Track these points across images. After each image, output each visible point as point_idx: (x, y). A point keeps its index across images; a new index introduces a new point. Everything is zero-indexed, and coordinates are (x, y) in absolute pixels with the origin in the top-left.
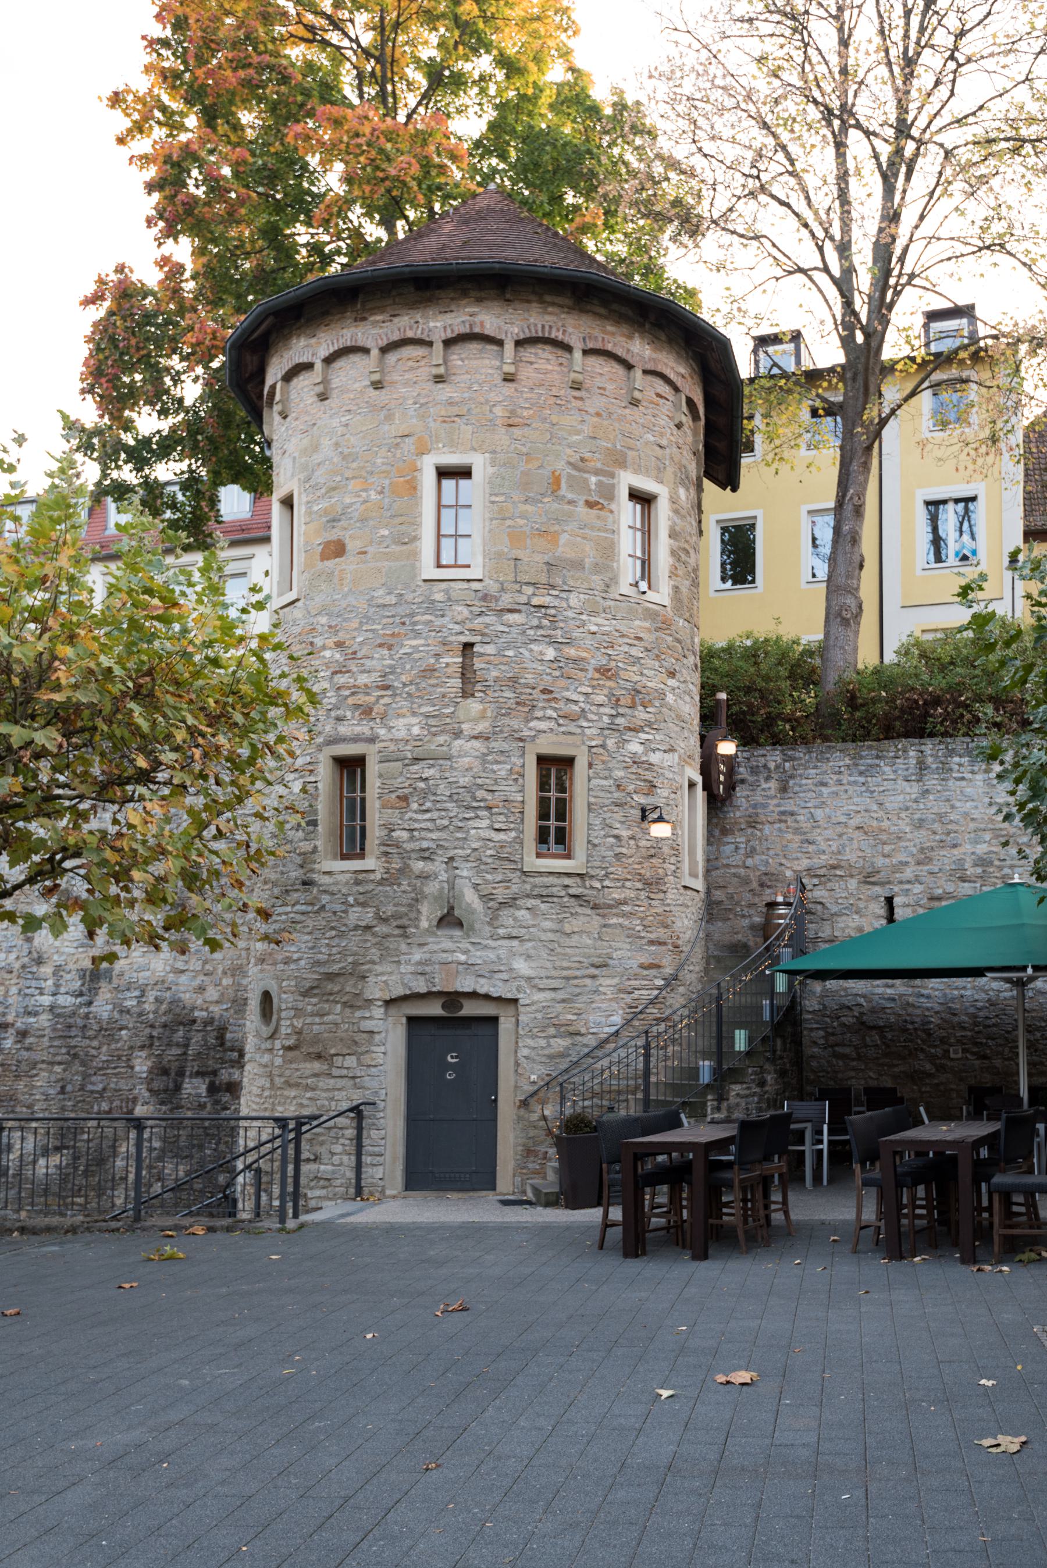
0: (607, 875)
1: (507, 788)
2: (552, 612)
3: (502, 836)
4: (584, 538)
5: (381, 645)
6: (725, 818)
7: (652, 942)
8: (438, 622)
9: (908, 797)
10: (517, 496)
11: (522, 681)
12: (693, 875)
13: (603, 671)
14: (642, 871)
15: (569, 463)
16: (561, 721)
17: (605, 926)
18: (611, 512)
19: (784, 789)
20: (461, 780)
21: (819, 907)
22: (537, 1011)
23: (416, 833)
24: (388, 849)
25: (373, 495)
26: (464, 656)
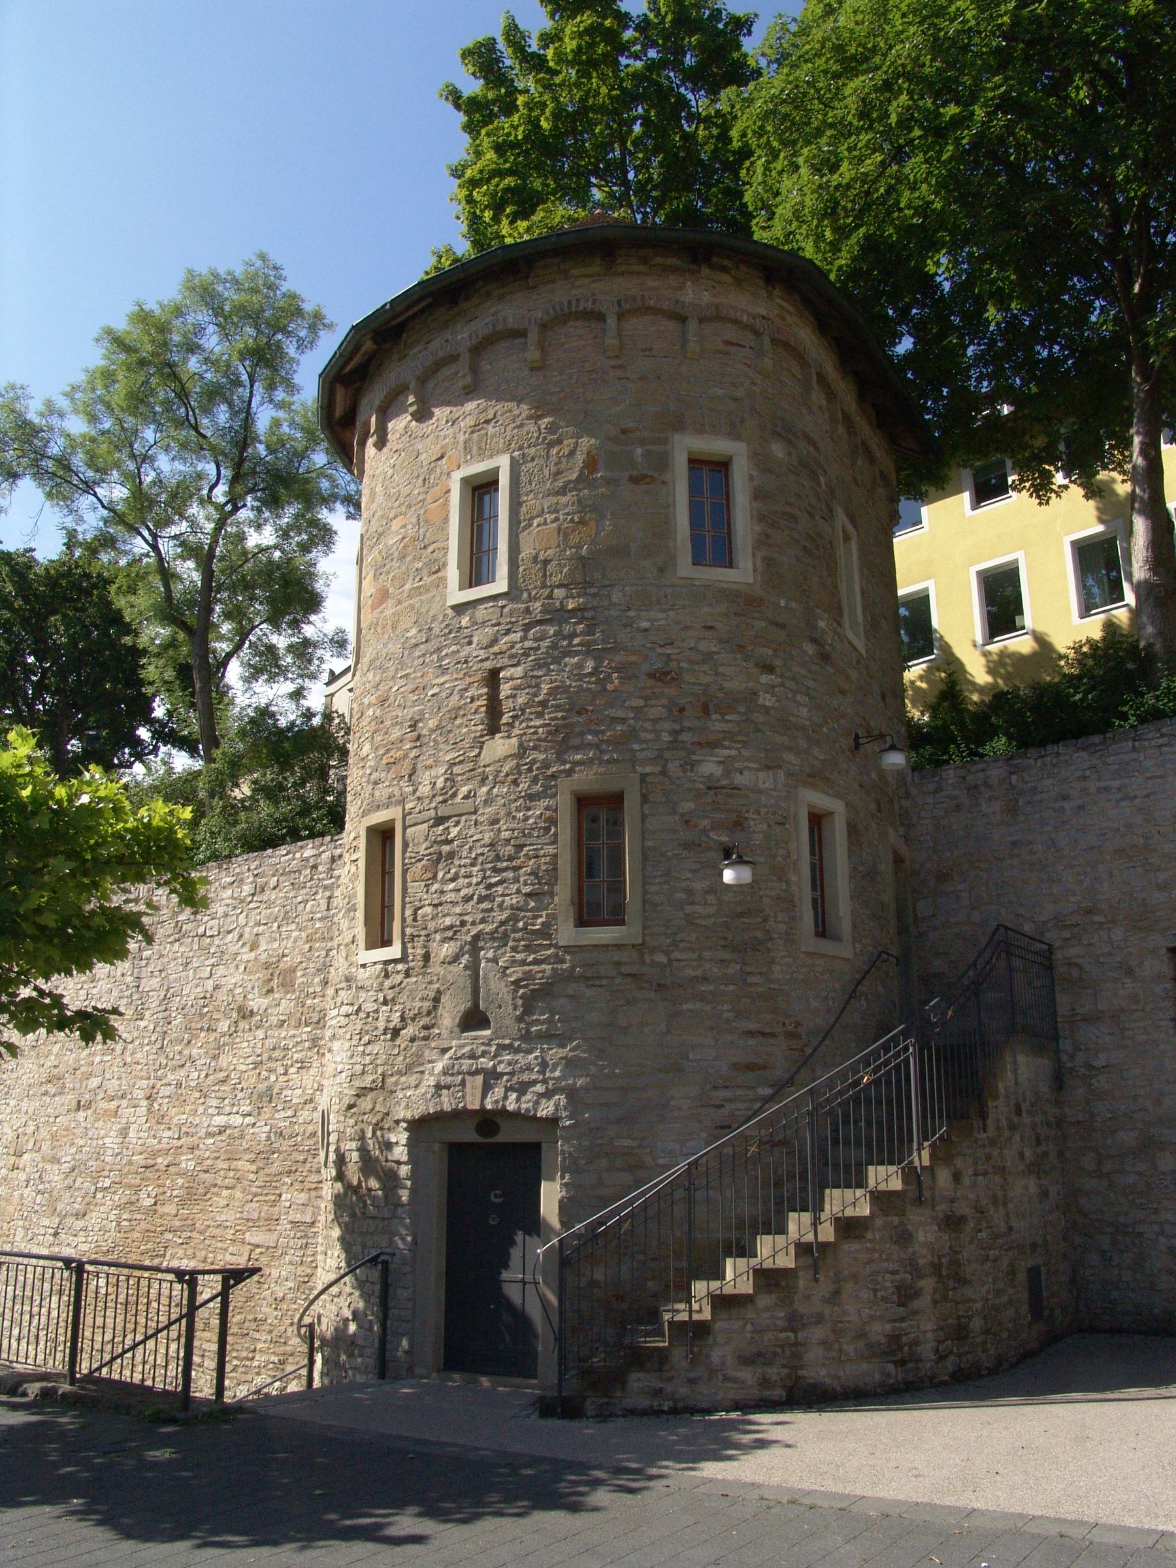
0: (675, 944)
7: (750, 1033)
13: (661, 676)
18: (664, 483)
19: (1012, 809)
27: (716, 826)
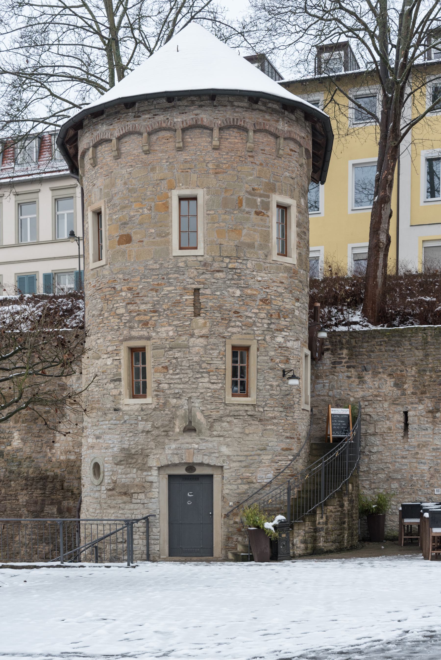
0: (266, 405)
1: (218, 362)
2: (239, 271)
3: (215, 386)
4: (255, 231)
5: (152, 290)
6: (318, 370)
7: (287, 438)
8: (181, 278)
9: (417, 358)
10: (221, 211)
11: (224, 307)
12: (306, 403)
13: (264, 301)
14: (283, 402)
15: (247, 192)
16: (244, 328)
17: (265, 430)
18: (268, 216)
20: (194, 359)
21: (368, 417)
22: (232, 472)
23: (171, 385)
24: (158, 393)
25: (146, 211)
26: (194, 295)
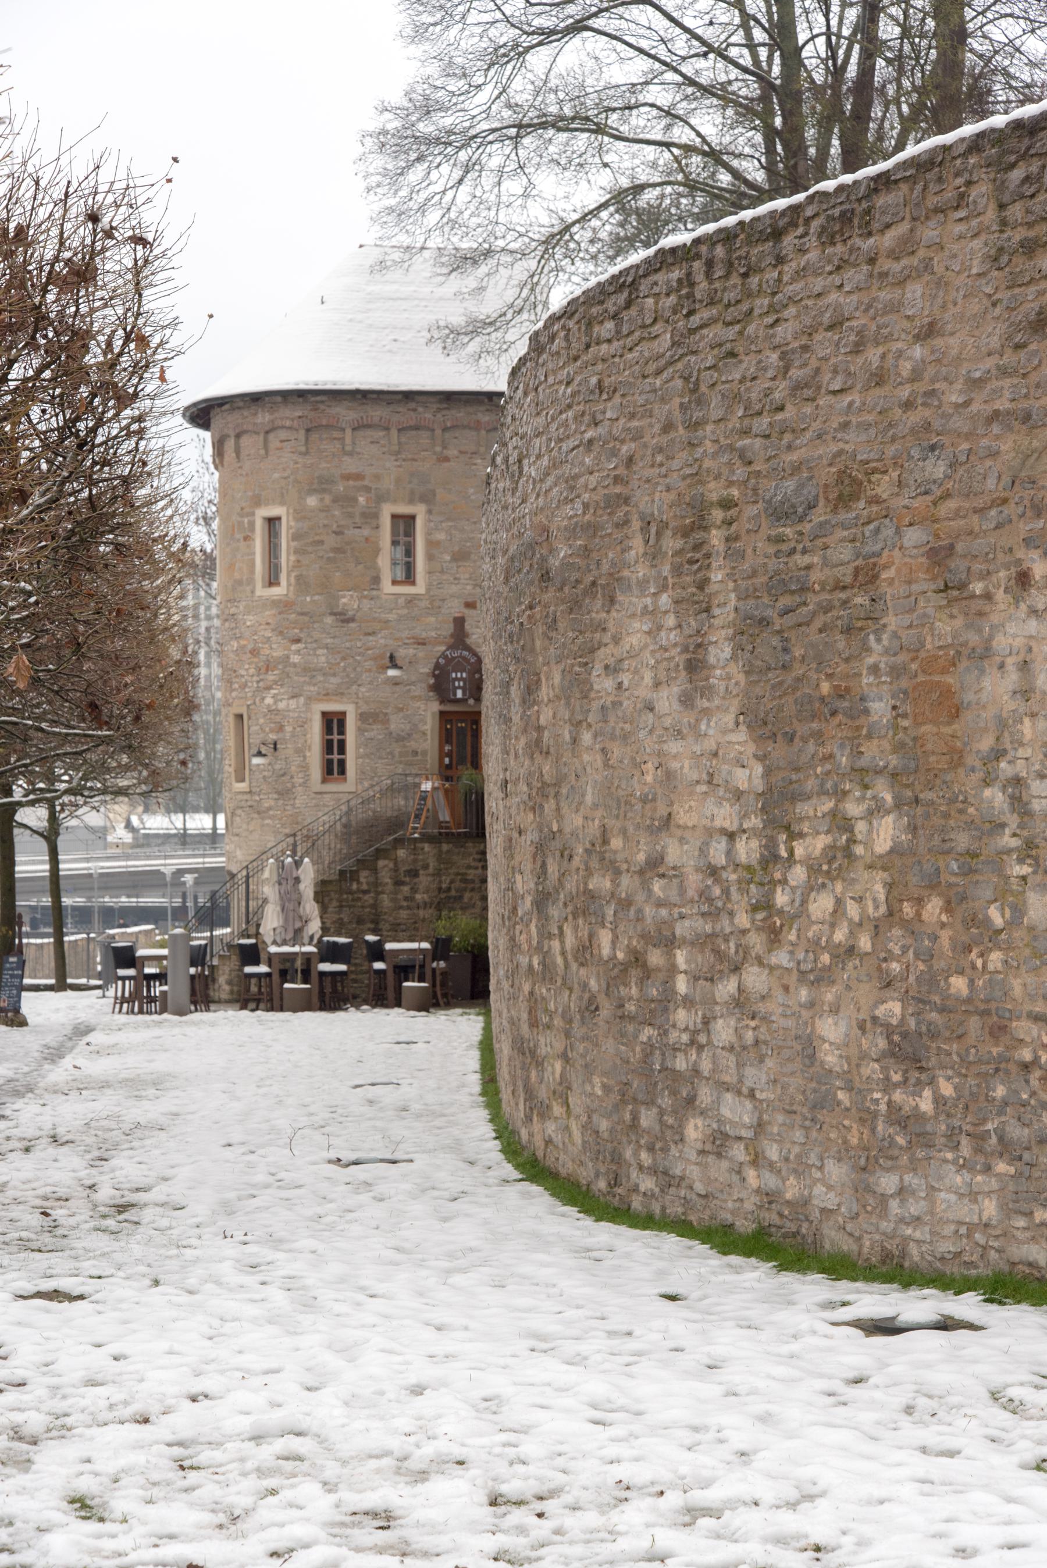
27: (272, 731)
